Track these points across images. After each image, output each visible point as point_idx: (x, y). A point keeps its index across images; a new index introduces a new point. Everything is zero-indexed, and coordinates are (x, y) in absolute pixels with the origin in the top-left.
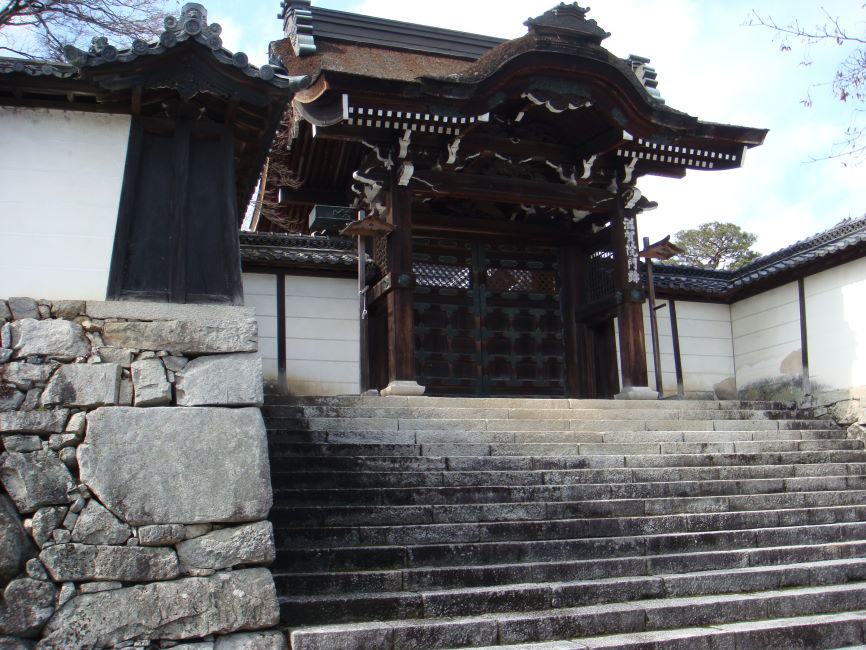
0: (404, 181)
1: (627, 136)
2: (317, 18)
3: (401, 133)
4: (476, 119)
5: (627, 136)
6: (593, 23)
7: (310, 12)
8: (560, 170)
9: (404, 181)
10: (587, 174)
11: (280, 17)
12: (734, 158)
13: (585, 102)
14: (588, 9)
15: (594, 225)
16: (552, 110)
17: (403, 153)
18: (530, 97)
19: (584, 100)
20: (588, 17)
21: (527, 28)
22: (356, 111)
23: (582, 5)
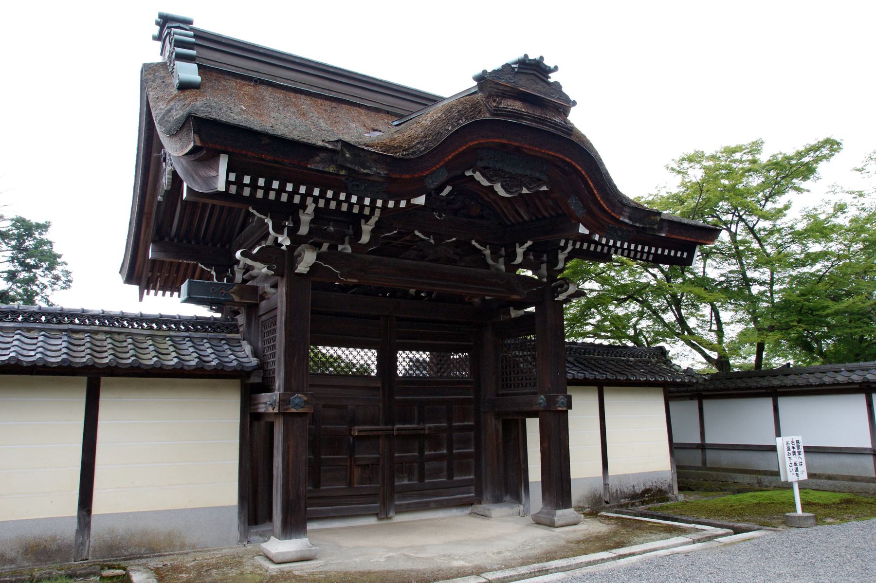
0: (302, 268)
1: (583, 230)
2: (200, 42)
3: (303, 206)
4: (408, 202)
5: (583, 230)
6: (557, 86)
7: (192, 33)
8: (487, 252)
9: (302, 268)
10: (365, 239)
11: (155, 38)
12: (685, 255)
13: (540, 186)
14: (556, 68)
15: (511, 308)
16: (502, 193)
17: (304, 230)
18: (478, 176)
19: (540, 182)
20: (553, 78)
21: (475, 83)
22: (239, 179)
23: (548, 62)
